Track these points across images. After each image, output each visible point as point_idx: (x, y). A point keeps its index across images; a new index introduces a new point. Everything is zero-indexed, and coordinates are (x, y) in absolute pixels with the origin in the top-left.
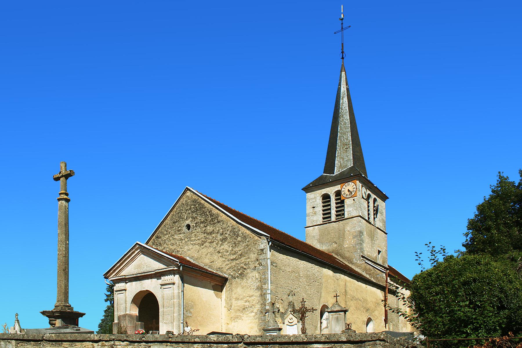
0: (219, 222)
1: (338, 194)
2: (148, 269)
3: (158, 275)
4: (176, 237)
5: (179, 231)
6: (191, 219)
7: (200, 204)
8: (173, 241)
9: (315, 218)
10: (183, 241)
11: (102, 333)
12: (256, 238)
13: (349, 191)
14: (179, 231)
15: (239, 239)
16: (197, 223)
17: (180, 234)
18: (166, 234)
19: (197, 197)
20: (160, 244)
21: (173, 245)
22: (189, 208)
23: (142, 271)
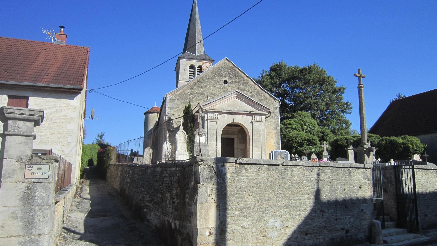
0: (249, 85)
1: (200, 67)
2: (241, 109)
3: (250, 114)
4: (215, 85)
5: (219, 82)
6: (228, 77)
7: (235, 71)
8: (213, 88)
9: (185, 77)
10: (222, 90)
11: (83, 147)
12: (273, 100)
13: (207, 67)
14: (219, 82)
15: (262, 98)
16: (232, 81)
17: (220, 84)
18: (207, 82)
19: (233, 66)
20: (202, 87)
21: (213, 90)
22: (227, 70)
23: (236, 109)
